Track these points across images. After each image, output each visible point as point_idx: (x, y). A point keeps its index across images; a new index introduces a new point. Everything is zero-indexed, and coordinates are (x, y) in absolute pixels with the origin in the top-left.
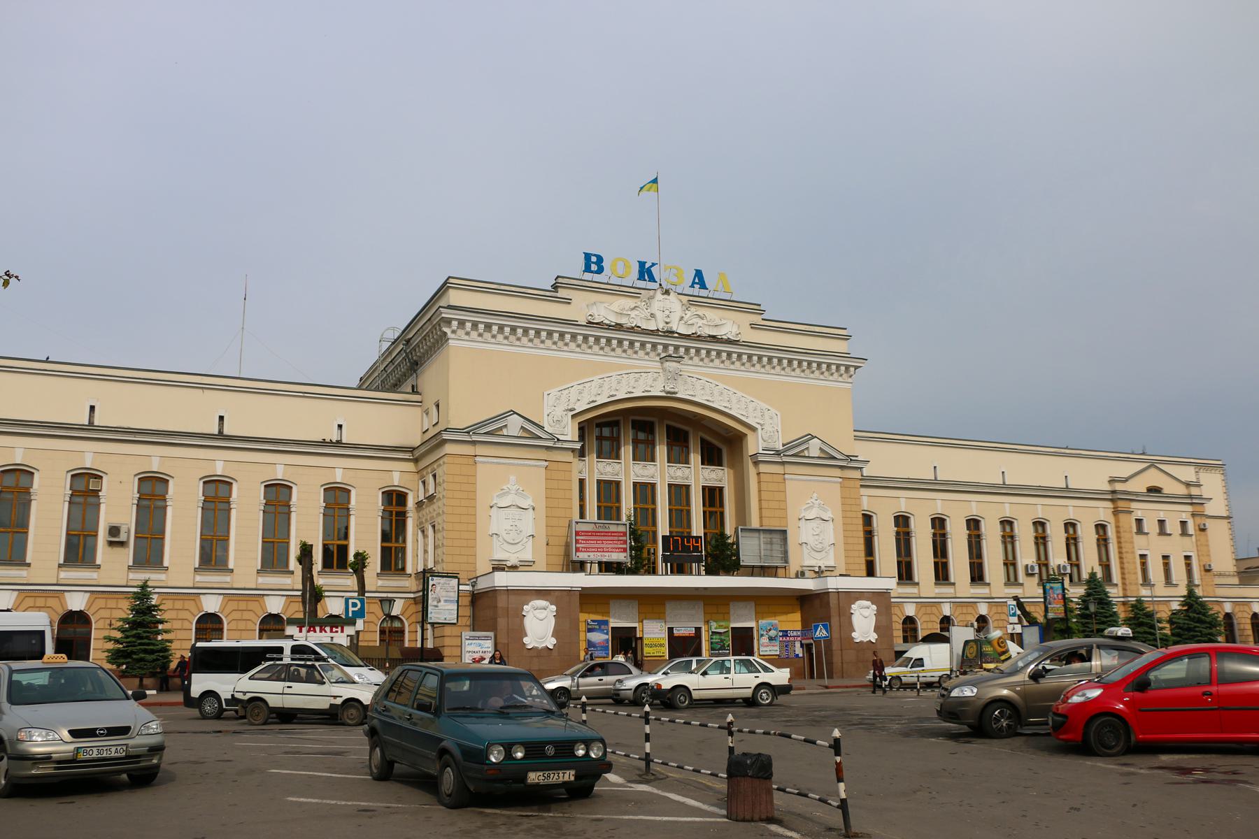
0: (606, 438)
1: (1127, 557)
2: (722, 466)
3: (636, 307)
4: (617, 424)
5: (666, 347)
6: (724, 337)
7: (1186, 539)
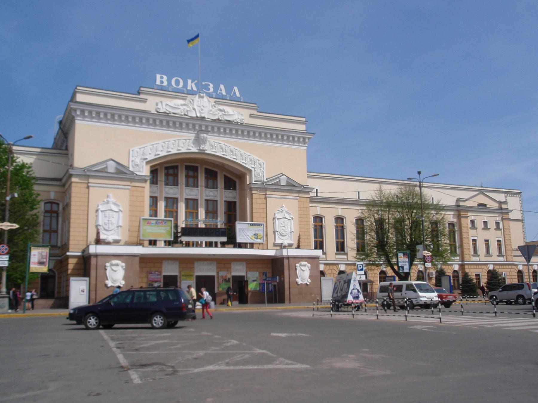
0: (170, 175)
1: (465, 241)
4: (176, 167)
6: (235, 121)
7: (499, 232)
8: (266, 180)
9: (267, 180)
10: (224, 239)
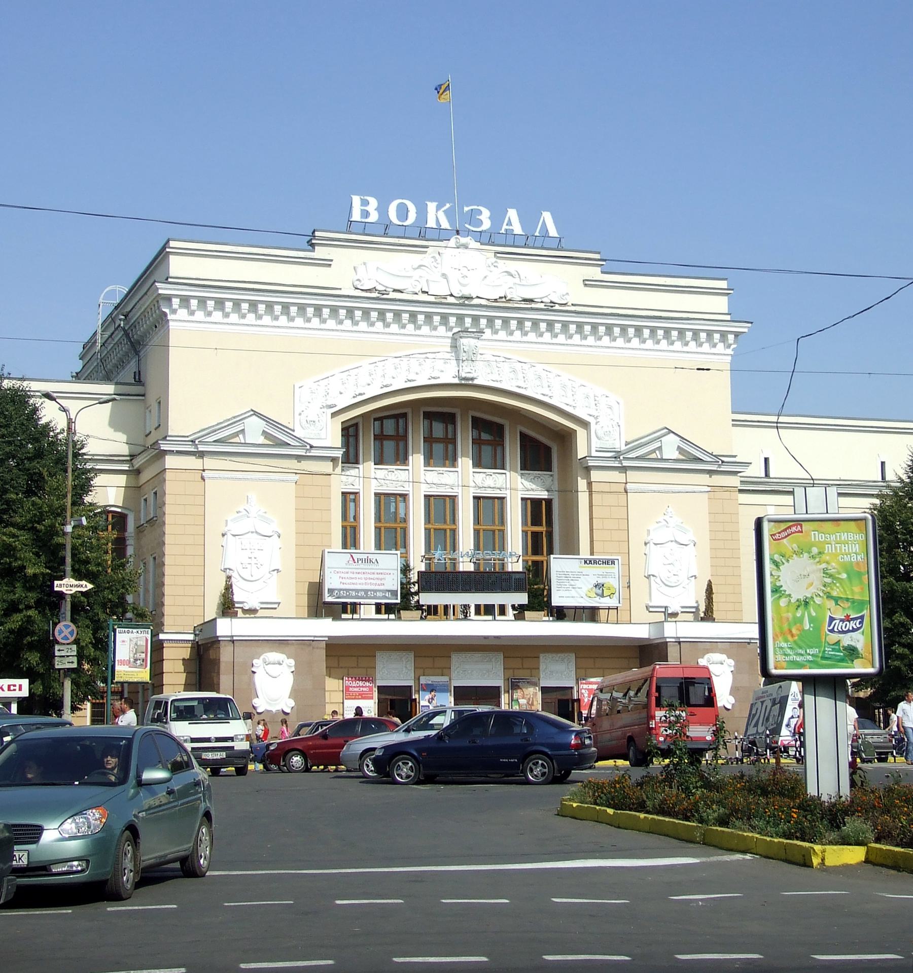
2: (503, 469)
3: (421, 266)
5: (460, 318)
8: (626, 445)
9: (628, 446)
10: (522, 598)
